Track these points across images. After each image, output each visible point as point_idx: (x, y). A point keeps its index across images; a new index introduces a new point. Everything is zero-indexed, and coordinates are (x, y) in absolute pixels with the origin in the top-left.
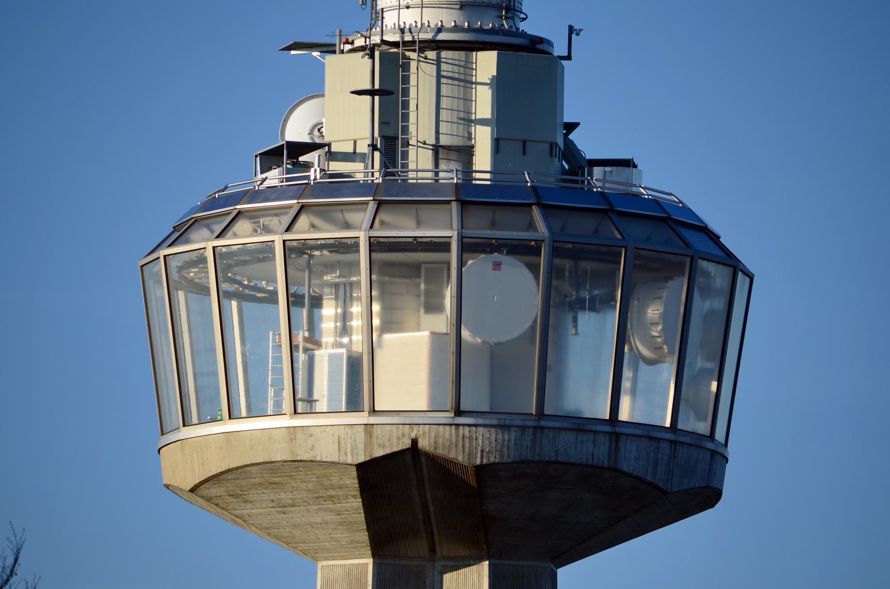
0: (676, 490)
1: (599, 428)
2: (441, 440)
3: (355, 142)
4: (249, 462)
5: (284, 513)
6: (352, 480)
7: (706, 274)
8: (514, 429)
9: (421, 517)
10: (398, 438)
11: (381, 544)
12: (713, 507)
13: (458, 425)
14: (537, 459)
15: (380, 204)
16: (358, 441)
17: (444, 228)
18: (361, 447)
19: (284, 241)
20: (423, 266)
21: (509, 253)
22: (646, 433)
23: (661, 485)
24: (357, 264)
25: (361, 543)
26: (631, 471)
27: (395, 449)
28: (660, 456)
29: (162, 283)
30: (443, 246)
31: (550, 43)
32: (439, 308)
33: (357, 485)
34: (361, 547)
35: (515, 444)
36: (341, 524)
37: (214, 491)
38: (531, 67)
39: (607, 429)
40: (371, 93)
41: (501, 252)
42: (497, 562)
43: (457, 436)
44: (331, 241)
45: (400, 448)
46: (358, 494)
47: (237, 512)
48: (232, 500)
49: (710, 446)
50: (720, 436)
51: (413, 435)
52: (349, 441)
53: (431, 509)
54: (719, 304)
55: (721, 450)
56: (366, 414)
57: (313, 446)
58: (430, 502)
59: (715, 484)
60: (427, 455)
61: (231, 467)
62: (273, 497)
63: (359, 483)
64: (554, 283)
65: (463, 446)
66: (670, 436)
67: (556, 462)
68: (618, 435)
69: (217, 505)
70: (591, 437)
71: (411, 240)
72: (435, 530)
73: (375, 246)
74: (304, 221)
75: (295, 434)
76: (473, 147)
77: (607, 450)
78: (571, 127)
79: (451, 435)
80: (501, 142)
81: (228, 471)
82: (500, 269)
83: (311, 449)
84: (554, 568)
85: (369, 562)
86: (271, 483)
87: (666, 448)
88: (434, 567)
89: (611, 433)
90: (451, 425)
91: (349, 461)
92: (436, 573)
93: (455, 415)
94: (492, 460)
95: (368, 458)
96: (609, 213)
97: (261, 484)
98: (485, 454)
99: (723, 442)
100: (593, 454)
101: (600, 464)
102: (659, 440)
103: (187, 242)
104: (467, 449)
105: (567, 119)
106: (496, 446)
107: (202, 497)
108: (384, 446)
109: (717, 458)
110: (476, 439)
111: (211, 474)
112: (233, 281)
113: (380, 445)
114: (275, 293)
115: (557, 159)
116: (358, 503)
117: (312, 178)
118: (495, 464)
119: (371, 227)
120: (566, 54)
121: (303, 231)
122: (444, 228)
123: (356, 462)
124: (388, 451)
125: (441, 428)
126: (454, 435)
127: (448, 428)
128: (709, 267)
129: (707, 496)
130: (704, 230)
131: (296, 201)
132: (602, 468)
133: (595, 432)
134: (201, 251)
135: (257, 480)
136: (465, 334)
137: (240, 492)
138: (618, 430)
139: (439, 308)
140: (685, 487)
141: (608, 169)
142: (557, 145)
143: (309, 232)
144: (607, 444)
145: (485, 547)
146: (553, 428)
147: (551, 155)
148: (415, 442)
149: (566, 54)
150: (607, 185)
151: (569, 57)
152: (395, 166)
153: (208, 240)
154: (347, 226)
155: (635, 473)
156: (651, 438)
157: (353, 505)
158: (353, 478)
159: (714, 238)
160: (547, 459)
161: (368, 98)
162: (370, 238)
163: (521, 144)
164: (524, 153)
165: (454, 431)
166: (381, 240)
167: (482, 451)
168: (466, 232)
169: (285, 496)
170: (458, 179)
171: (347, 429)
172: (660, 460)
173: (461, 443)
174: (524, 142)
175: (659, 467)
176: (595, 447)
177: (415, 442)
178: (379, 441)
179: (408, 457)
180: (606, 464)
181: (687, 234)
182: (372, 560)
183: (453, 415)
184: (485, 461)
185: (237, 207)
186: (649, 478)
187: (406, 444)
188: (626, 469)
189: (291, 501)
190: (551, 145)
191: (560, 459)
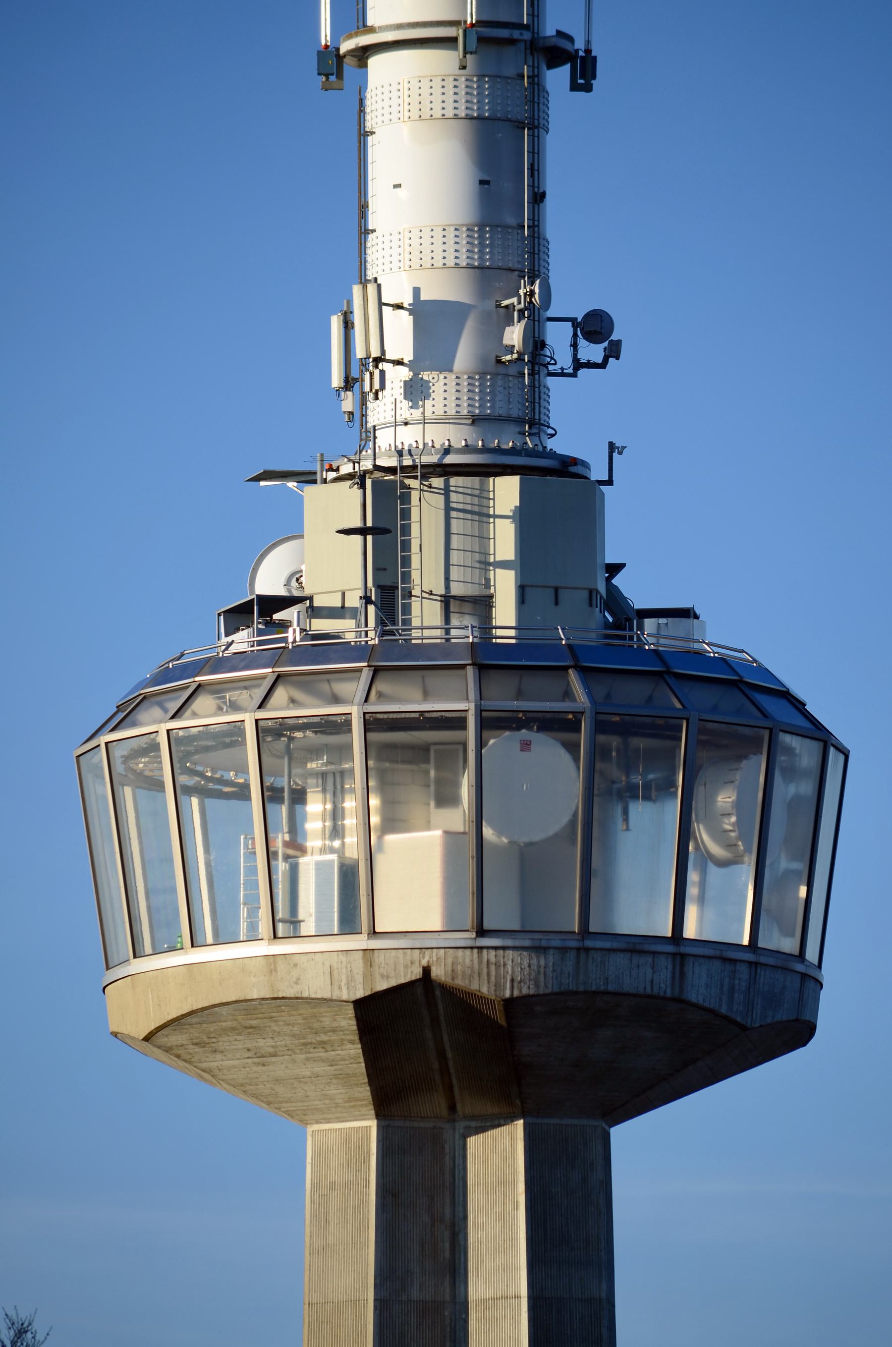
0: (757, 1025)
3: (343, 594)
5: (264, 1065)
6: (348, 1022)
7: (789, 751)
8: (551, 952)
9: (436, 1066)
10: (406, 967)
11: (386, 1102)
12: (804, 1045)
13: (480, 948)
14: (581, 988)
16: (355, 971)
18: (359, 978)
19: (257, 721)
22: (718, 953)
23: (739, 1020)
24: (350, 747)
25: (361, 1100)
26: (701, 1002)
27: (402, 981)
29: (103, 778)
30: (456, 722)
33: (355, 1028)
34: (362, 1106)
35: (554, 971)
36: (336, 1076)
37: (173, 1038)
39: (670, 949)
41: (530, 729)
42: (534, 1120)
43: (480, 962)
45: (408, 979)
46: (356, 1038)
47: (204, 1065)
48: (197, 1049)
49: (800, 968)
50: (811, 955)
51: (424, 962)
52: (344, 971)
53: (449, 1055)
54: (807, 788)
55: (813, 972)
56: (364, 936)
57: (298, 979)
59: (807, 1017)
60: (443, 987)
62: (248, 1045)
64: (599, 765)
65: (488, 974)
67: (607, 993)
68: (683, 956)
69: (178, 1056)
70: (650, 959)
71: (416, 715)
73: (371, 723)
74: (281, 694)
75: (275, 963)
76: (491, 597)
77: (669, 975)
78: (614, 569)
79: (472, 961)
80: (528, 591)
83: (296, 983)
84: (607, 1127)
85: (373, 1124)
86: (246, 1027)
87: (744, 972)
88: (454, 1129)
89: (674, 955)
90: (472, 948)
92: (457, 1136)
93: (477, 936)
94: (525, 991)
95: (368, 993)
97: (233, 1029)
98: (516, 985)
99: (816, 963)
101: (662, 994)
102: (734, 961)
103: (134, 725)
104: (493, 979)
106: (530, 974)
107: (159, 1047)
108: (388, 977)
109: (809, 983)
110: (505, 965)
112: (193, 772)
113: (382, 976)
114: (246, 787)
115: (598, 609)
119: (366, 700)
121: (281, 708)
122: (459, 700)
123: (353, 998)
124: (393, 983)
125: (460, 952)
126: (476, 961)
127: (468, 952)
129: (798, 1032)
130: (786, 695)
131: (270, 670)
132: (664, 998)
133: (654, 953)
135: (229, 1024)
136: (488, 832)
137: (207, 1040)
138: (683, 950)
140: (769, 1020)
141: (662, 621)
142: (597, 592)
143: (287, 708)
144: (670, 967)
145: (518, 1102)
147: (591, 605)
148: (427, 971)
149: (606, 478)
150: (662, 641)
151: (610, 482)
152: (394, 622)
154: (336, 699)
155: (706, 1005)
156: (725, 960)
159: (799, 705)
160: (594, 988)
161: (358, 538)
162: (365, 714)
163: (552, 592)
164: (557, 603)
167: (512, 981)
168: (486, 704)
169: (264, 1044)
171: (341, 957)
172: (737, 988)
173: (485, 971)
174: (556, 590)
175: (736, 996)
176: (654, 972)
177: (427, 971)
179: (419, 990)
180: (669, 994)
183: (474, 935)
185: (197, 679)
186: (724, 1010)
187: (416, 973)
188: (694, 1000)
189: (272, 1050)
191: (611, 988)
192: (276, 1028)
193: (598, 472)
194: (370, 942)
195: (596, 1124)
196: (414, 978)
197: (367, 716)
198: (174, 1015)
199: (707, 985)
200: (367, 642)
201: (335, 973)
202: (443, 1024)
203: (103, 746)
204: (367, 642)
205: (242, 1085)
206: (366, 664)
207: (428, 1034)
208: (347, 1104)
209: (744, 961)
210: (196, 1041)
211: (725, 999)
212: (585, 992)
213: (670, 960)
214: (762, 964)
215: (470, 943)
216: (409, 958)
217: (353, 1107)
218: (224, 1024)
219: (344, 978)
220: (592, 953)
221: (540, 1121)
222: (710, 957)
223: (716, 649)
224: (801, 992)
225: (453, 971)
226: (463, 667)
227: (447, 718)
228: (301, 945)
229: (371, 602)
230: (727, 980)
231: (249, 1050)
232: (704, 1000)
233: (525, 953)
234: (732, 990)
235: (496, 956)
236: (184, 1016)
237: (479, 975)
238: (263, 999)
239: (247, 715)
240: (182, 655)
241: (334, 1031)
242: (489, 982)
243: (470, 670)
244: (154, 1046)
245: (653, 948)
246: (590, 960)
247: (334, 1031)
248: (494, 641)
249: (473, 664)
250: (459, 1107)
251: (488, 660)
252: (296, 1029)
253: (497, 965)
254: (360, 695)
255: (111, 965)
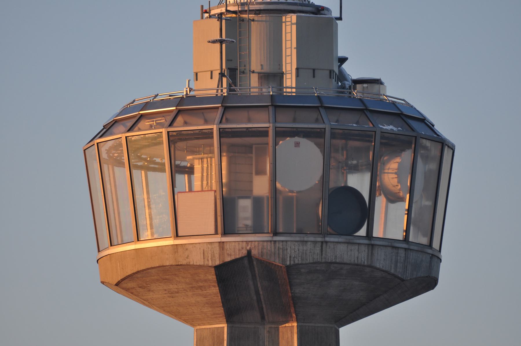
0: (409, 278)
1: (362, 241)
2: (265, 250)
3: (212, 72)
4: (150, 267)
5: (172, 297)
6: (212, 276)
7: (425, 148)
8: (309, 243)
9: (255, 298)
10: (239, 250)
11: (231, 314)
12: (433, 289)
13: (275, 242)
14: (323, 260)
15: (226, 109)
16: (215, 252)
17: (261, 122)
18: (217, 256)
19: (168, 132)
20: (254, 146)
21: (304, 137)
22: (390, 244)
23: (400, 276)
24: (212, 145)
25: (219, 314)
27: (238, 257)
28: (399, 258)
29: (96, 160)
30: (264, 133)
31: (328, 9)
32: (264, 173)
33: (215, 279)
34: (220, 317)
35: (310, 252)
36: (207, 303)
37: (130, 284)
38: (320, 26)
39: (366, 242)
40: (221, 42)
41: (299, 136)
42: (302, 324)
43: (275, 248)
44: (197, 131)
45: (240, 256)
46: (216, 285)
47: (144, 297)
48: (141, 290)
49: (430, 251)
50: (436, 245)
51: (248, 248)
52: (210, 252)
53: (261, 293)
54: (433, 166)
55: (436, 254)
56: (219, 236)
58: (260, 289)
59: (433, 275)
61: (139, 270)
62: (165, 288)
63: (217, 278)
64: (333, 155)
65: (279, 254)
66: (404, 246)
67: (336, 263)
68: (373, 245)
69: (132, 293)
70: (357, 247)
71: (245, 130)
72: (264, 306)
73: (223, 133)
74: (180, 119)
75: (177, 249)
77: (366, 255)
78: (343, 60)
79: (271, 247)
80: (299, 70)
81: (138, 272)
82: (299, 146)
83: (187, 258)
84: (337, 328)
85: (225, 326)
86: (164, 279)
87: (402, 253)
88: (264, 328)
89: (368, 245)
90: (271, 241)
91: (210, 264)
92: (266, 332)
93: (273, 236)
94: (296, 262)
95: (221, 263)
96: (365, 111)
97: (158, 280)
98: (292, 259)
99: (438, 249)
100: (358, 258)
101: (362, 263)
102: (398, 248)
103: (112, 134)
104: (281, 256)
105: (341, 53)
106: (299, 254)
107: (123, 289)
108: (231, 255)
109: (435, 258)
110: (287, 249)
111: (128, 274)
112: (140, 158)
113: (228, 254)
114: (164, 164)
115: (334, 80)
116: (215, 290)
117: (185, 93)
118: (298, 264)
119: (220, 122)
120: (339, 16)
121: (179, 127)
122: (265, 122)
123: (214, 265)
124: (233, 258)
125: (265, 244)
126: (273, 247)
128: (428, 143)
129: (429, 283)
130: (423, 120)
131: (175, 108)
132: (364, 266)
133: (359, 244)
134: (120, 140)
135: (156, 277)
136: (278, 185)
137: (145, 285)
139: (264, 173)
140: (415, 276)
141: (365, 85)
142: (334, 71)
143: (183, 126)
144: (366, 251)
145: (294, 315)
146: (333, 242)
147: (330, 77)
148: (249, 252)
149: (339, 16)
150: (365, 95)
151: (340, 19)
152: (236, 86)
153: (123, 133)
154: (206, 122)
155: (384, 269)
156: (393, 247)
157: (214, 291)
158: (213, 275)
159: (431, 127)
160: (330, 261)
161: (218, 45)
162: (220, 129)
163: (312, 71)
164: (314, 77)
165: (273, 245)
166: (227, 130)
167: (290, 257)
168: (278, 125)
169: (173, 287)
170: (273, 92)
171: (208, 245)
172: (399, 261)
173: (277, 252)
174: (314, 70)
175: (399, 264)
176: (359, 253)
177: (249, 252)
178: (228, 252)
179: (246, 261)
181: (414, 124)
182: (226, 325)
183: (272, 235)
184: (292, 263)
185: (141, 112)
186: (392, 271)
187: (244, 252)
188: (378, 267)
189: (176, 290)
190: (330, 71)
191: (338, 261)
192: (178, 280)
193: (335, 14)
194: (222, 238)
195: (332, 326)
196: (243, 256)
197: (221, 130)
198: (129, 273)
199: (384, 260)
200: (222, 95)
201: (206, 253)
202: (258, 277)
203: (96, 144)
204: (222, 95)
205: (163, 307)
206: (220, 105)
207: (251, 283)
208: (213, 316)
209: (402, 248)
210: (140, 286)
211: (393, 266)
212: (326, 263)
213: (366, 247)
214: (411, 250)
215: (269, 239)
216: (241, 246)
217: (216, 317)
218: (153, 278)
219: (210, 255)
220: (329, 244)
221: (305, 324)
222: (386, 246)
223: (390, 99)
224: (430, 262)
225: (262, 252)
226: (267, 106)
227: (259, 131)
228: (190, 240)
229: (225, 76)
230: (394, 257)
231: (165, 290)
232: (383, 267)
233: (296, 244)
234: (396, 262)
235: (282, 245)
236: (134, 274)
237: (275, 254)
238: (171, 265)
239: (164, 129)
240: (134, 101)
241: (206, 281)
242: (279, 258)
243: (271, 108)
244: (121, 288)
245: (358, 241)
246: (328, 247)
247: (206, 281)
248: (285, 94)
249: (272, 105)
250: (266, 317)
251: (278, 104)
252: (187, 280)
253: (283, 250)
254: (218, 120)
255: (100, 249)
